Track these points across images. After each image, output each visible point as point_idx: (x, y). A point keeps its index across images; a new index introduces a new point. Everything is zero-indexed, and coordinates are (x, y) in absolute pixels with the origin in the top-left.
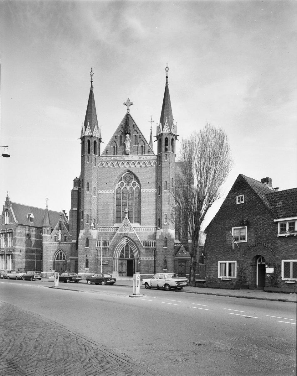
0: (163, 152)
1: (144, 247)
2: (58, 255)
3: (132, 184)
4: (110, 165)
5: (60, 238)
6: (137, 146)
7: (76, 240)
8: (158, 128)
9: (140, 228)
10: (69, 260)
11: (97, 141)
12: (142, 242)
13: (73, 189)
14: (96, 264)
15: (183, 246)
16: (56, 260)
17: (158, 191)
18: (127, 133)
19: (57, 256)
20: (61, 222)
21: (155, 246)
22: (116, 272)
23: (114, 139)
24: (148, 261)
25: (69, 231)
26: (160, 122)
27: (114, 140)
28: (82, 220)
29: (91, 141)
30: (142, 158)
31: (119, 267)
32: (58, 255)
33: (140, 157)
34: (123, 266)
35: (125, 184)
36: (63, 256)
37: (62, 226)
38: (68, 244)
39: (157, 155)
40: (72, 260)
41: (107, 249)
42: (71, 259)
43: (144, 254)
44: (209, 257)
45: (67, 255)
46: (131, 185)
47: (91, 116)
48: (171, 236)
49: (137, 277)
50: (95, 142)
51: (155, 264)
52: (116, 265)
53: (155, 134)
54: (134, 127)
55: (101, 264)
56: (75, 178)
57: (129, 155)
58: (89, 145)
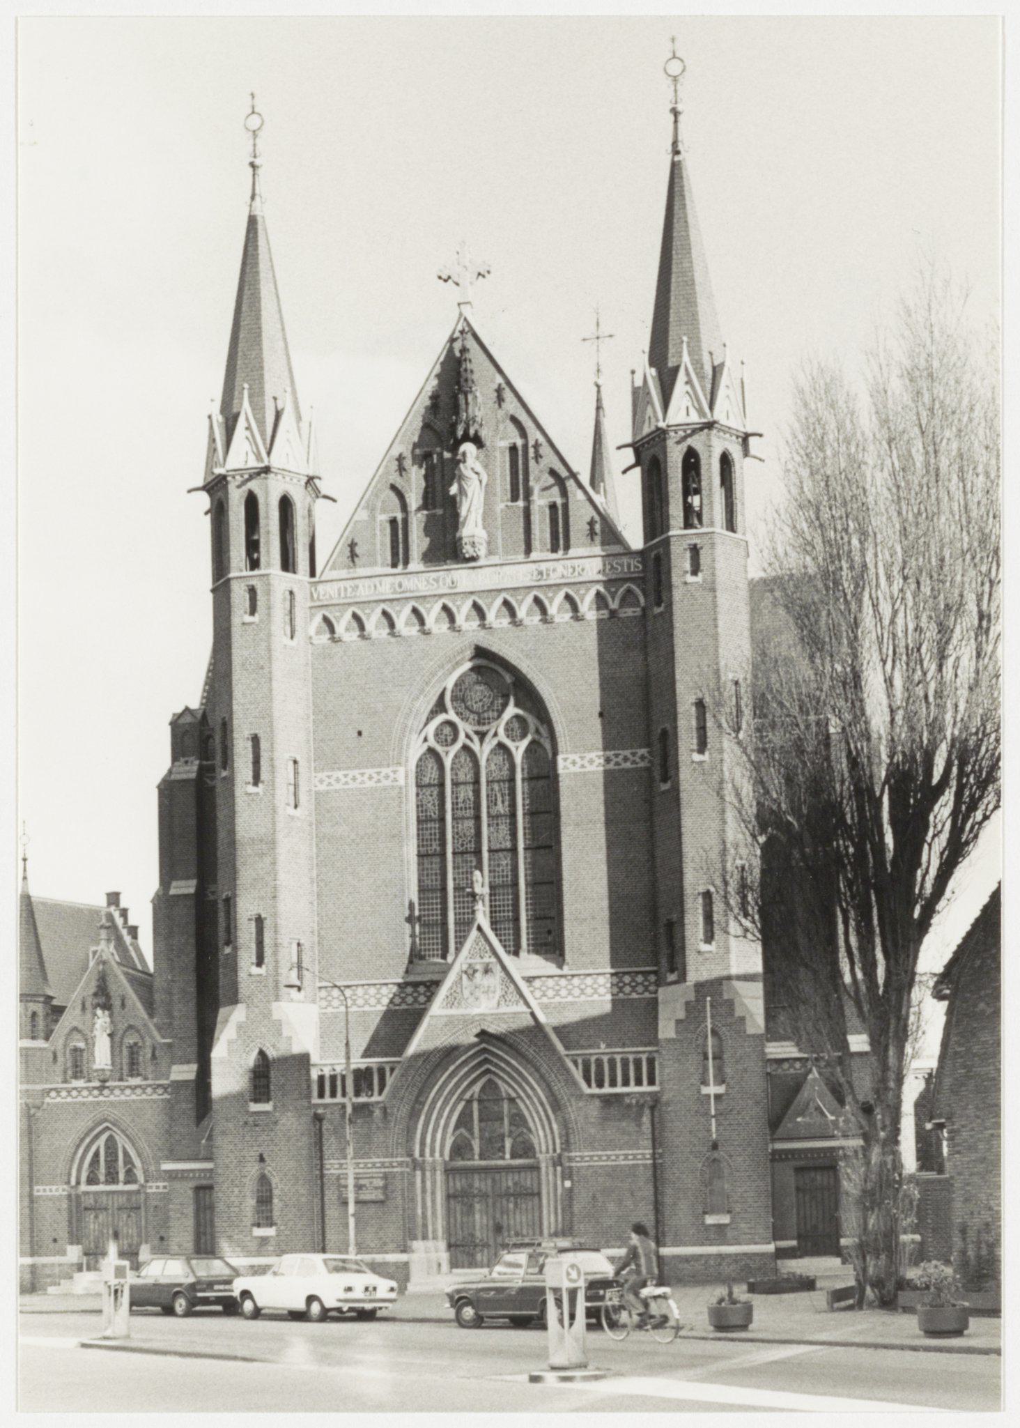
0: (676, 529)
1: (588, 1091)
2: (97, 1154)
3: (506, 730)
4: (528, 614)
5: (102, 1056)
6: (521, 503)
7: (194, 1067)
8: (639, 397)
9: (563, 982)
10: (157, 1180)
12: (575, 1063)
13: (170, 772)
14: (317, 1200)
15: (815, 1074)
16: (84, 1187)
17: (657, 761)
18: (466, 438)
19: (91, 1164)
20: (104, 963)
22: (430, 1244)
23: (395, 478)
26: (652, 364)
28: (228, 950)
29: (261, 501)
30: (558, 574)
31: (449, 1212)
32: (97, 1154)
33: (543, 566)
34: (471, 1206)
35: (464, 727)
36: (125, 1163)
37: (113, 989)
38: (149, 1090)
39: (641, 553)
40: (177, 1185)
42: (172, 1176)
43: (593, 1131)
44: (965, 1134)
45: (148, 1151)
46: (501, 731)
47: (260, 358)
48: (742, 1019)
49: (568, 1274)
50: (286, 504)
51: (656, 1188)
52: (433, 1201)
53: (619, 429)
54: (500, 399)
55: (345, 1203)
56: (179, 710)
57: (481, 562)
58: (246, 526)
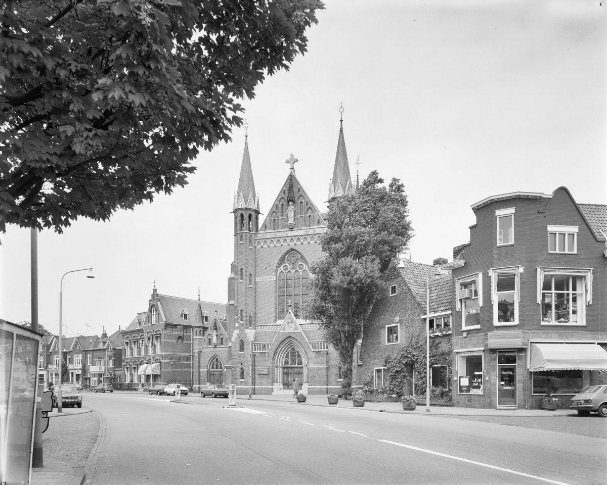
11: (253, 214)
16: (211, 370)
21: (327, 348)
24: (318, 369)
25: (226, 331)
27: (272, 213)
31: (283, 377)
32: (214, 362)
33: (307, 230)
35: (289, 267)
41: (267, 354)
